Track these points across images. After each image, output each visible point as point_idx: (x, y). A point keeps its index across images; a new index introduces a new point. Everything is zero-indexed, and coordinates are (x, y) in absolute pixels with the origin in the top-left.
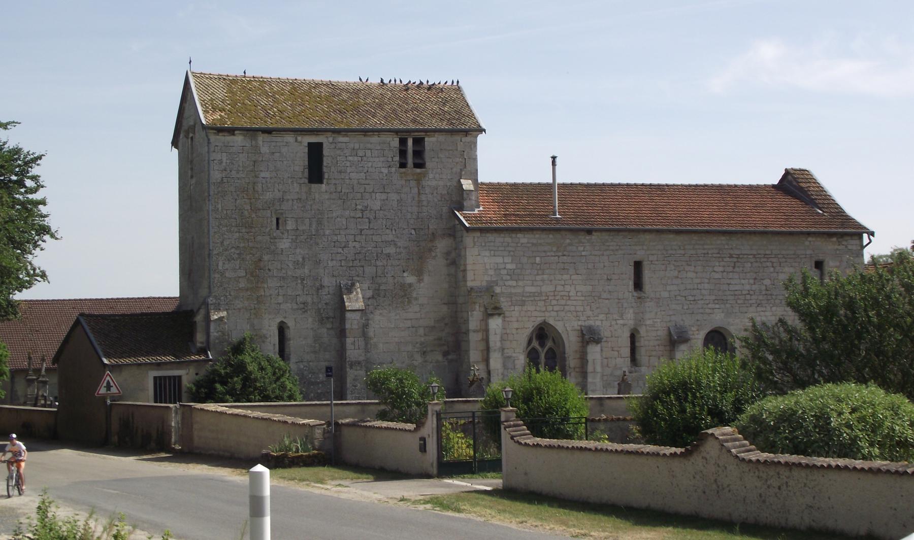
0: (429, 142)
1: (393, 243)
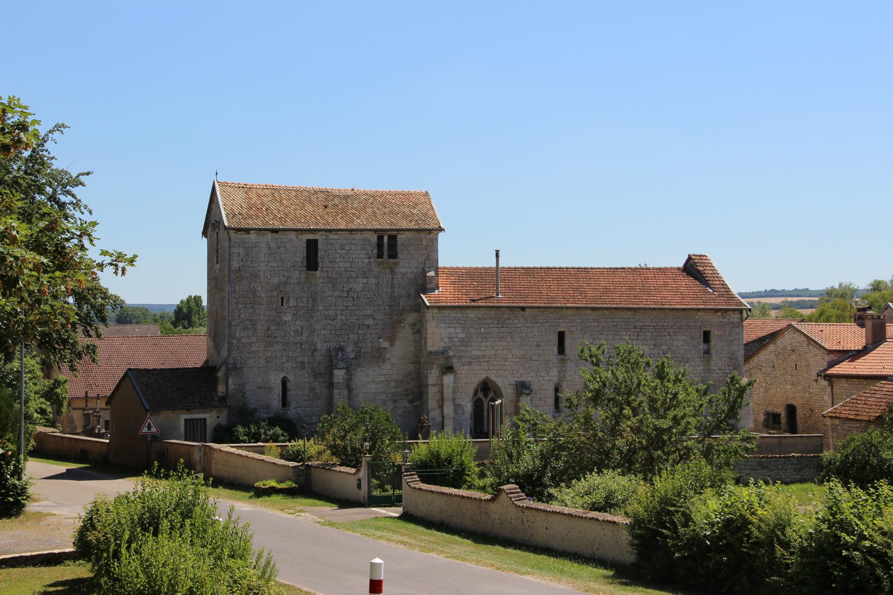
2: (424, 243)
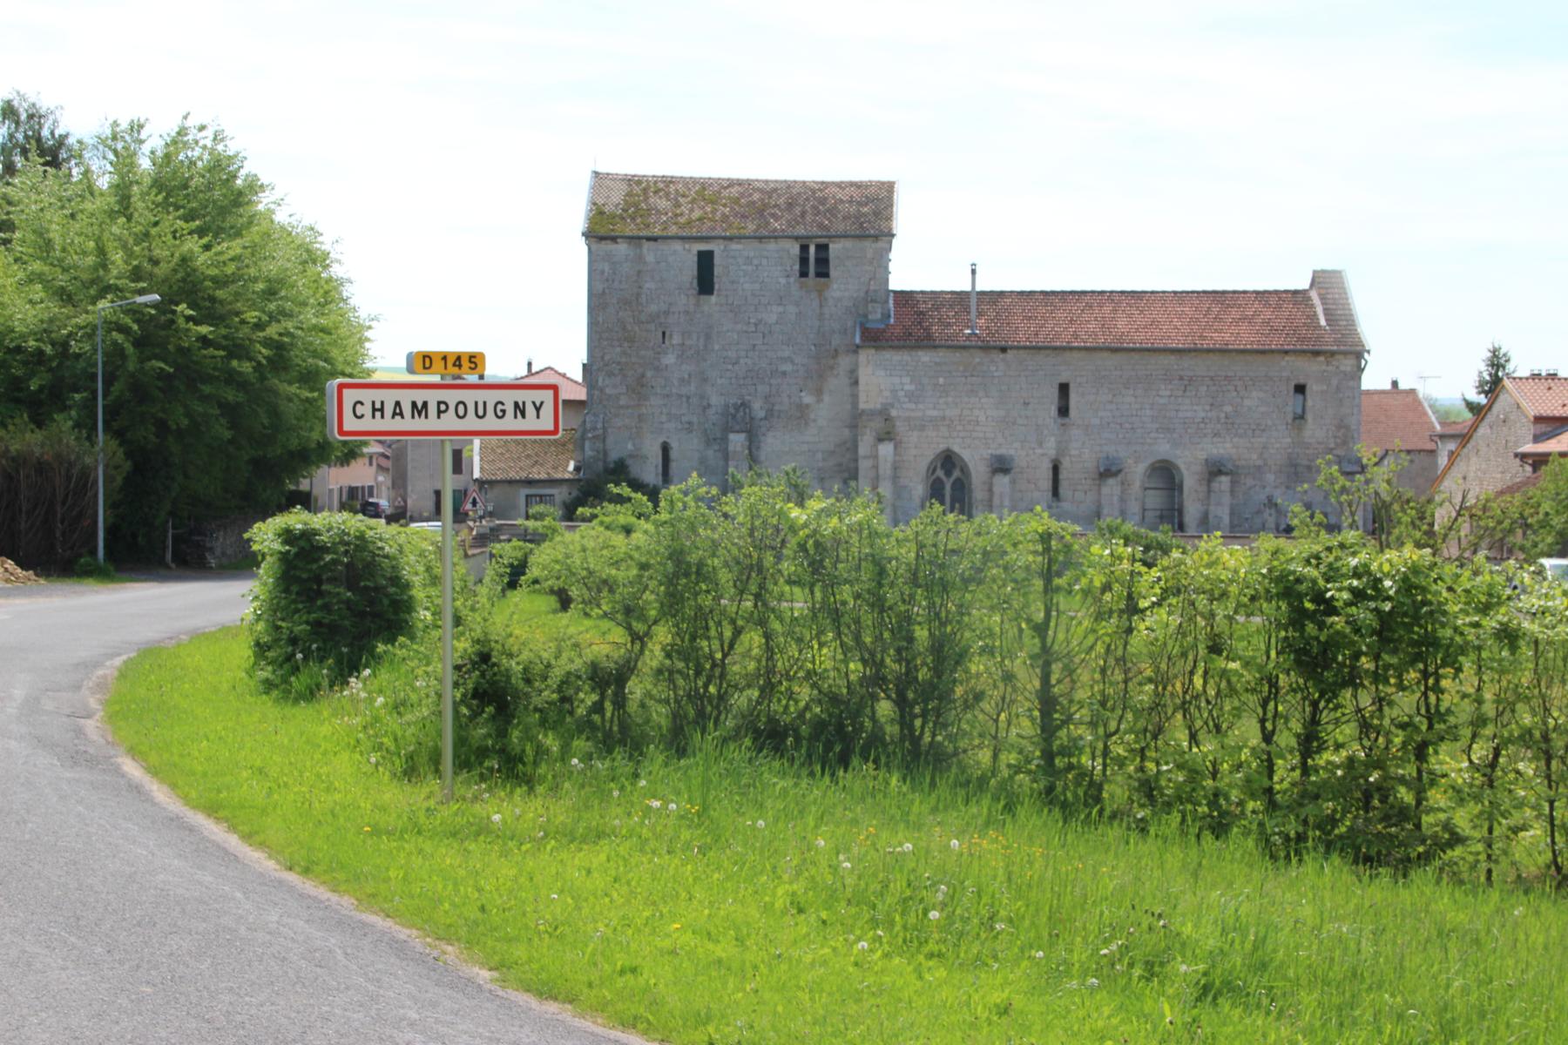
0: (835, 248)
1: (790, 360)
2: (869, 255)
